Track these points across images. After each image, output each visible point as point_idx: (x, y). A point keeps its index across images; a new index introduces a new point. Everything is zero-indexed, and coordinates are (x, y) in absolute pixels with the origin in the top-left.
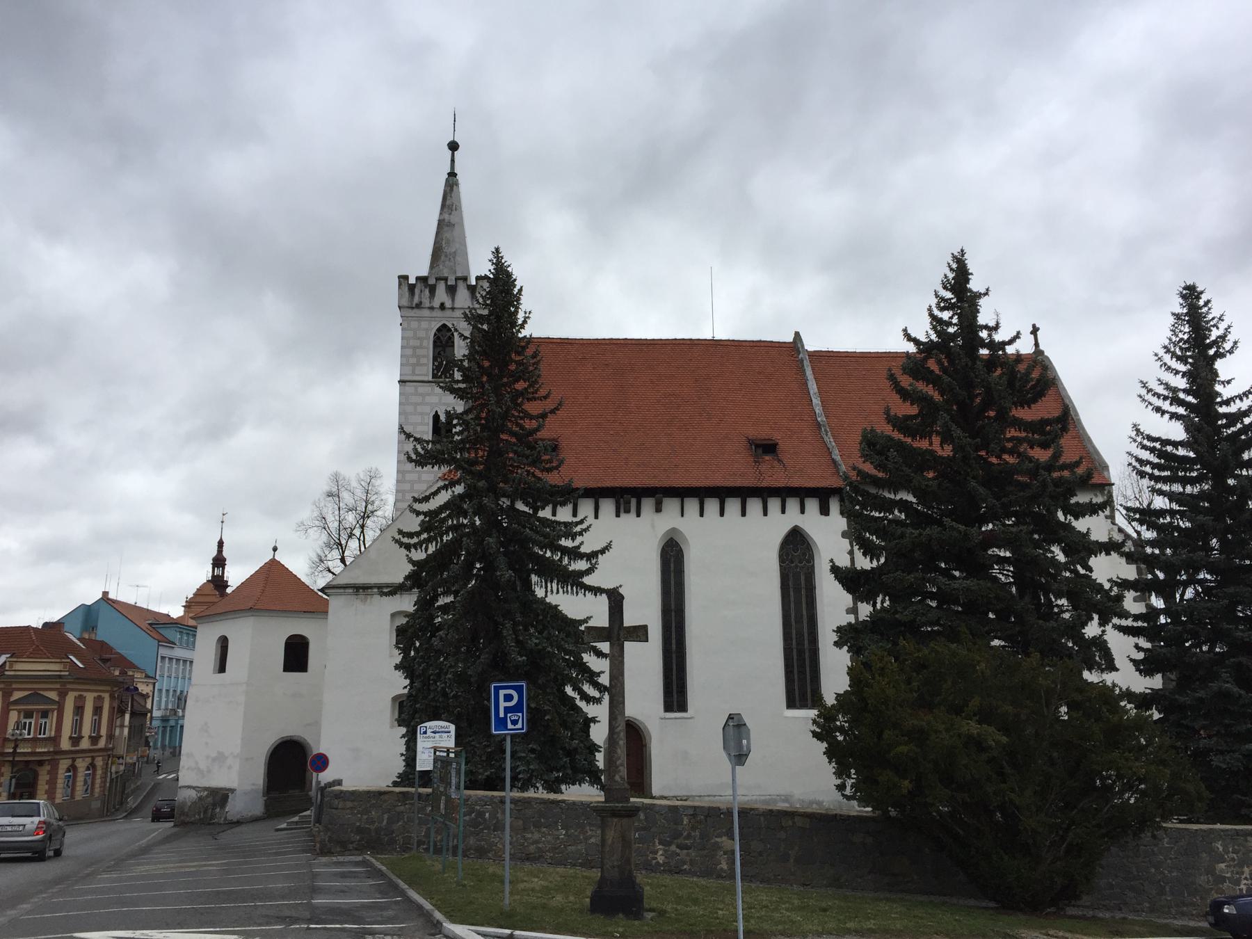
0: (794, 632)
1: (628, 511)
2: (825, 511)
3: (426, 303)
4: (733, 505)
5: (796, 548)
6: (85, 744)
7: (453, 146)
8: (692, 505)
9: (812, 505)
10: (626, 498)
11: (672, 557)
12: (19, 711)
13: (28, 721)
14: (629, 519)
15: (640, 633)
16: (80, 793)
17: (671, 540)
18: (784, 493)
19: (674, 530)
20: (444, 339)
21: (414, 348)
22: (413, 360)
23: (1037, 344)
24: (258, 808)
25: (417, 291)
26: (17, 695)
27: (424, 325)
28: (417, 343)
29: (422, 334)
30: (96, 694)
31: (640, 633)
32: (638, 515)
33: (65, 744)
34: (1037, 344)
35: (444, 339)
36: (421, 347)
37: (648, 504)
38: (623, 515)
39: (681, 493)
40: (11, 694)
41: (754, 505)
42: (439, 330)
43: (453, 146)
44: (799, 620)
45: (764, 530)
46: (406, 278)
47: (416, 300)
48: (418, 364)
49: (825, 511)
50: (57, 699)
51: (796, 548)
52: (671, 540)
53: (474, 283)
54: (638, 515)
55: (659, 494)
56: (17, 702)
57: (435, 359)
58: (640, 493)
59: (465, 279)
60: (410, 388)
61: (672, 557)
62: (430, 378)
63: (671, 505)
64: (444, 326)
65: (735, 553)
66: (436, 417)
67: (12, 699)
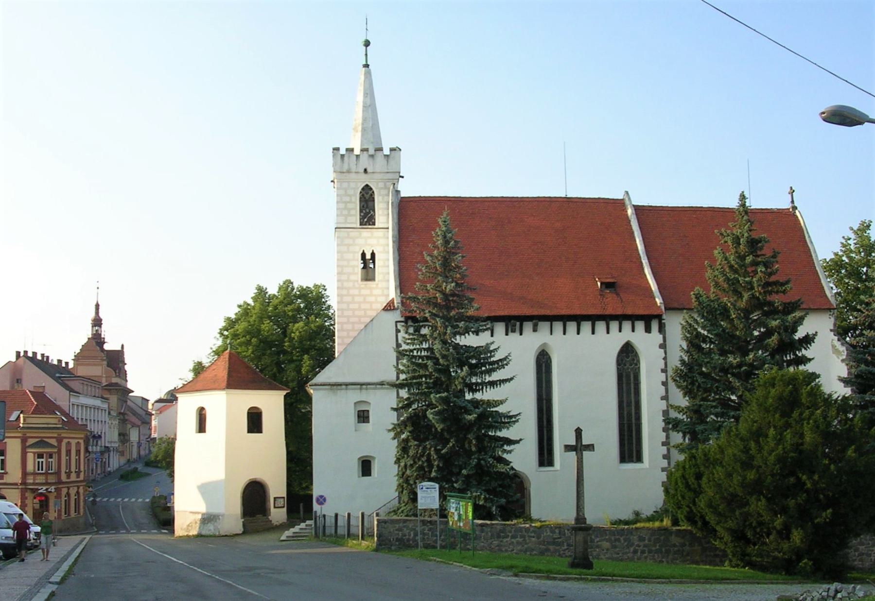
0: (625, 413)
1: (513, 331)
2: (648, 330)
3: (354, 169)
4: (586, 326)
5: (628, 356)
6: (73, 477)
7: (367, 44)
8: (558, 326)
9: (640, 326)
10: (514, 322)
11: (543, 362)
12: (34, 453)
13: (41, 460)
14: (514, 337)
15: (568, 448)
16: (73, 514)
17: (543, 351)
18: (621, 318)
19: (545, 344)
20: (367, 196)
21: (346, 203)
22: (345, 212)
23: (793, 202)
24: (239, 529)
25: (346, 158)
26: (31, 441)
27: (352, 185)
28: (348, 199)
29: (351, 192)
30: (77, 441)
31: (568, 448)
32: (521, 334)
33: (64, 478)
34: (793, 202)
35: (367, 196)
36: (350, 202)
37: (528, 326)
38: (510, 334)
39: (551, 319)
40: (26, 441)
41: (601, 326)
42: (363, 189)
43: (367, 44)
44: (629, 404)
45: (605, 343)
46: (337, 149)
47: (346, 167)
48: (349, 215)
49: (648, 330)
50: (56, 444)
51: (628, 356)
52: (543, 351)
53: (388, 153)
54: (521, 334)
55: (536, 320)
56: (32, 446)
57: (361, 211)
58: (523, 319)
59: (381, 149)
60: (343, 233)
61: (543, 362)
62: (358, 226)
63: (544, 326)
64: (367, 185)
65: (585, 358)
66: (363, 255)
67: (28, 444)
